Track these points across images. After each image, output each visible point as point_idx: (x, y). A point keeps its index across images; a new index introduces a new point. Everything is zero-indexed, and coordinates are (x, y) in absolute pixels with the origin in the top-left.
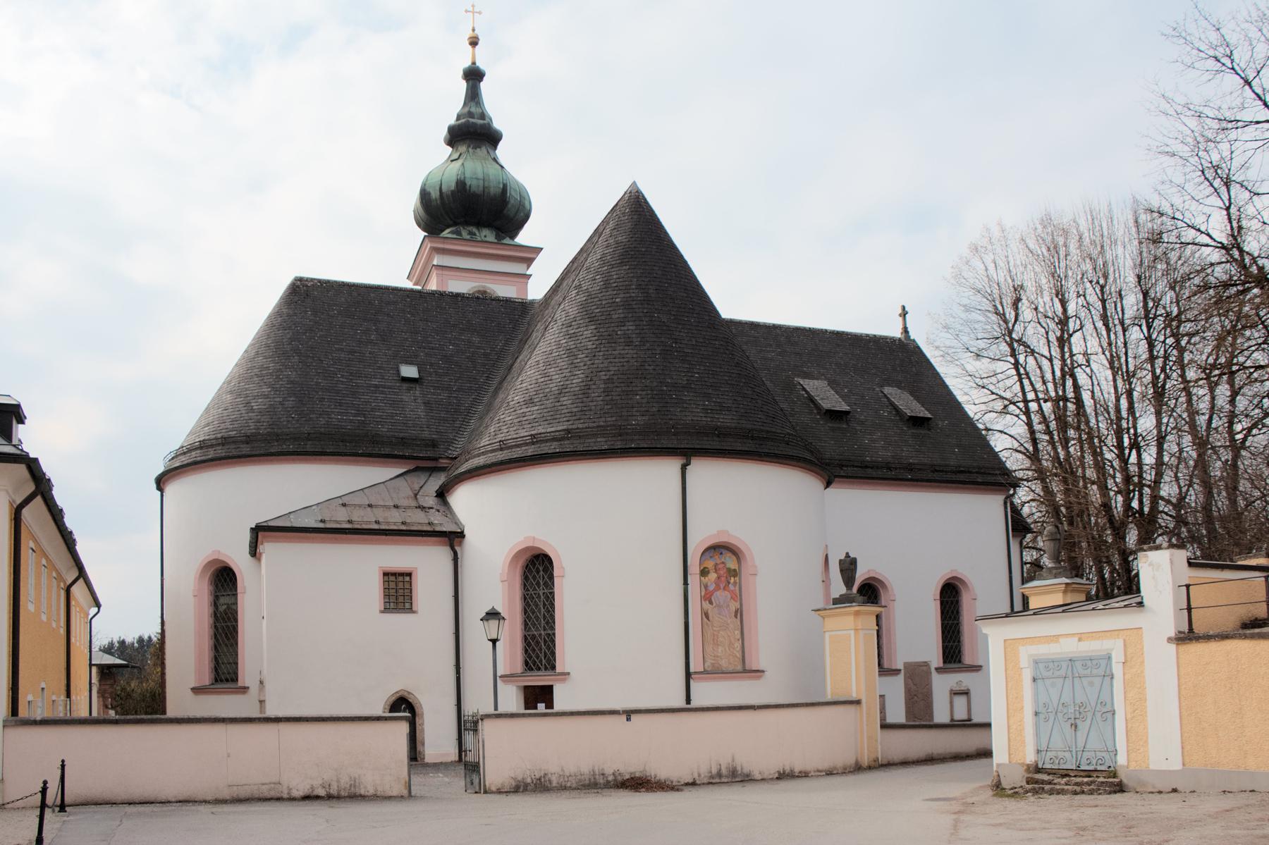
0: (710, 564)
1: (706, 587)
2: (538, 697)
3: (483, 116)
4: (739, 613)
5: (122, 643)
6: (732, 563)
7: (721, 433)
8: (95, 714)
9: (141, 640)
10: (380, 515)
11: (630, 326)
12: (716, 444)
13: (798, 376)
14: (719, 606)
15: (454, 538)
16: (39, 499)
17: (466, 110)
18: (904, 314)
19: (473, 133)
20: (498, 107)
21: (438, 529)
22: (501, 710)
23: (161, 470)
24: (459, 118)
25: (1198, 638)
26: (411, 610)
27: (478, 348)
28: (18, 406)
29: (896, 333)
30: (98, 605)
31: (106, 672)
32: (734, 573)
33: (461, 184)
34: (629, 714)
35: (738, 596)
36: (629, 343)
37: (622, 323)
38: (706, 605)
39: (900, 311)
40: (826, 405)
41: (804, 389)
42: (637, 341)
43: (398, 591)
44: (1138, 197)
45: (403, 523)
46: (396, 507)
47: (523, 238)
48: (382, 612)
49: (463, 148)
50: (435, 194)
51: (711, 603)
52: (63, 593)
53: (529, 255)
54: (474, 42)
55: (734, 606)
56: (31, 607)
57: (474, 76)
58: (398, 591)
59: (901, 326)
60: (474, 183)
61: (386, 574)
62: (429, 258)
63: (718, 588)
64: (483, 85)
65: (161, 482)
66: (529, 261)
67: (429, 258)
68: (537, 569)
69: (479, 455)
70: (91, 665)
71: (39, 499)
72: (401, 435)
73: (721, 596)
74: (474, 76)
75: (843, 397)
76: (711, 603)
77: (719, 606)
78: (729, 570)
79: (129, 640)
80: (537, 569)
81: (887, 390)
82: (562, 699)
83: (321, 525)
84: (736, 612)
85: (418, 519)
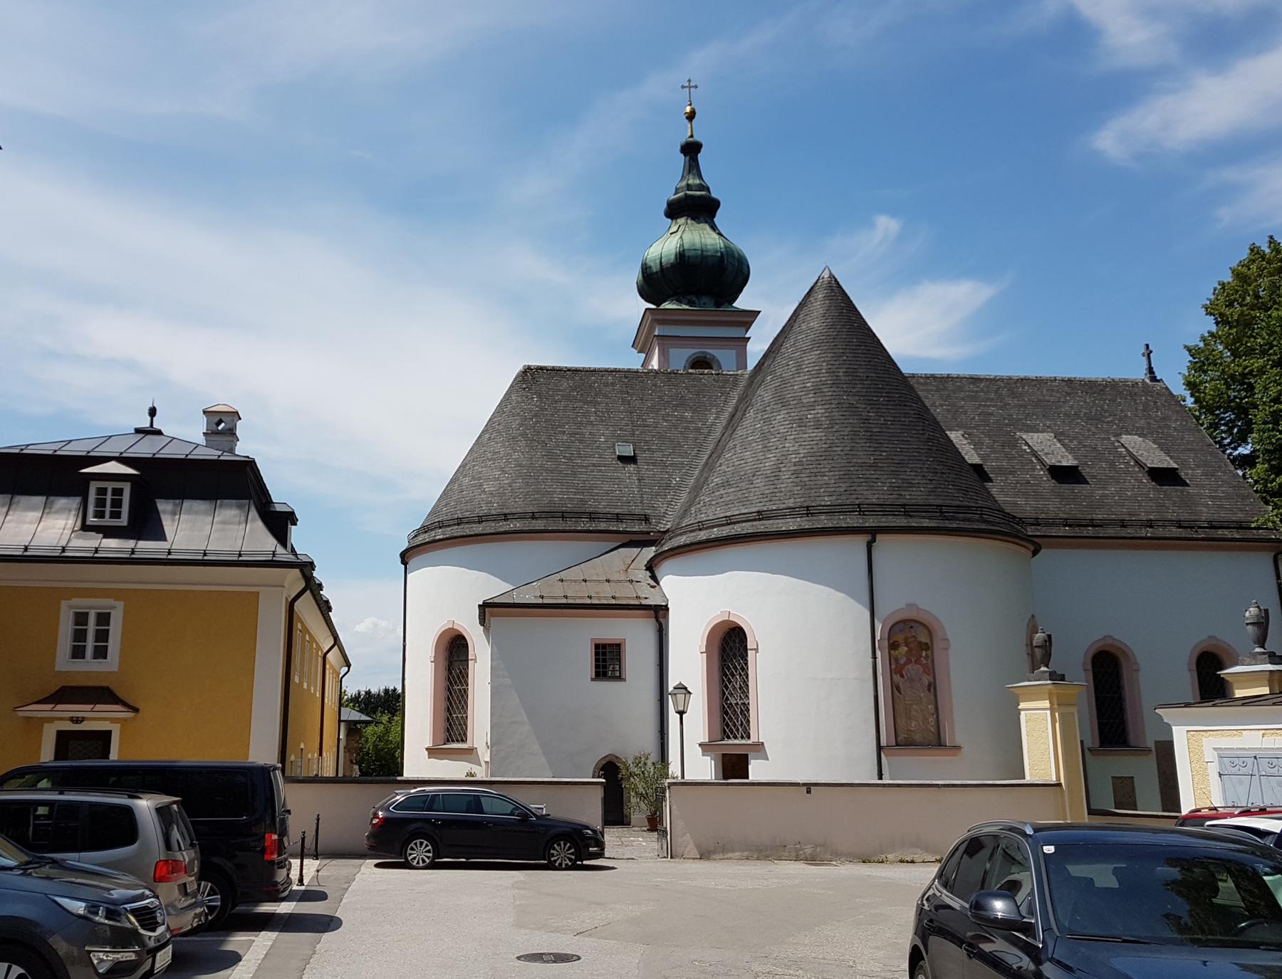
0: (900, 638)
1: (897, 660)
2: (734, 767)
3: (703, 187)
4: (932, 687)
5: (368, 693)
6: (923, 638)
7: (907, 510)
8: (340, 775)
9: (386, 691)
10: (591, 589)
11: (820, 410)
12: (902, 522)
13: (1020, 430)
14: (911, 680)
15: (659, 613)
16: (308, 592)
17: (684, 183)
18: (1148, 354)
19: (695, 206)
20: (716, 176)
21: (644, 602)
22: (688, 777)
23: (405, 545)
24: (677, 192)
25: (804, 784)
26: (620, 678)
27: (690, 422)
28: (293, 513)
29: (1140, 374)
30: (349, 665)
31: (353, 729)
32: (927, 647)
33: (682, 256)
34: (809, 787)
35: (930, 670)
36: (818, 426)
37: (811, 407)
38: (897, 678)
39: (1143, 350)
40: (1051, 461)
41: (1027, 444)
42: (826, 423)
43: (607, 661)
44: (1191, 344)
45: (613, 598)
46: (608, 581)
47: (742, 303)
48: (592, 680)
49: (682, 221)
50: (655, 268)
51: (902, 676)
52: (320, 660)
53: (749, 317)
54: (691, 116)
55: (926, 680)
56: (297, 680)
57: (691, 150)
58: (607, 661)
59: (1145, 366)
60: (692, 253)
61: (597, 646)
62: (651, 329)
63: (908, 662)
64: (701, 157)
65: (405, 557)
66: (748, 325)
67: (651, 329)
68: (730, 646)
69: (681, 534)
70: (340, 721)
71: (308, 592)
72: (617, 511)
73: (912, 669)
74: (691, 150)
75: (1071, 450)
76: (902, 676)
77: (911, 680)
78: (920, 643)
79: (374, 690)
80: (730, 646)
81: (1125, 439)
82: (757, 770)
83: (540, 601)
84: (929, 686)
85: (626, 594)
